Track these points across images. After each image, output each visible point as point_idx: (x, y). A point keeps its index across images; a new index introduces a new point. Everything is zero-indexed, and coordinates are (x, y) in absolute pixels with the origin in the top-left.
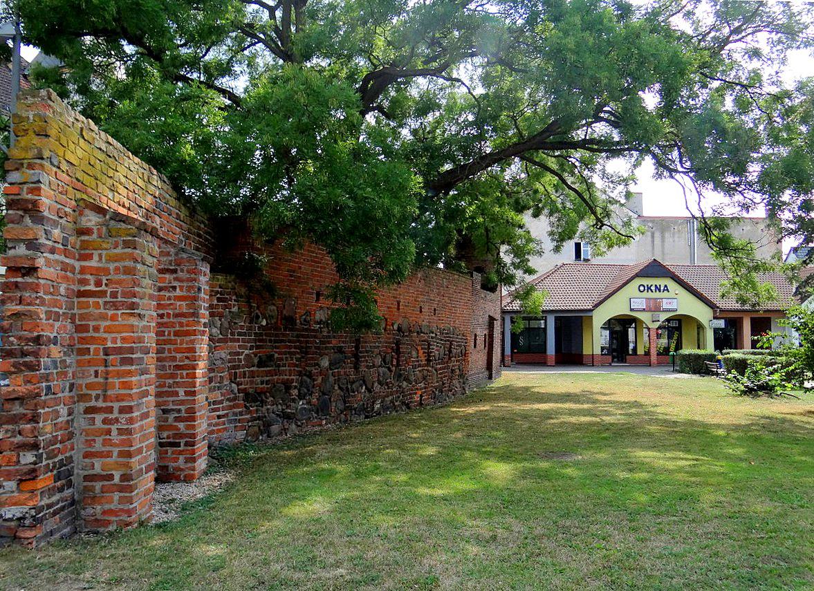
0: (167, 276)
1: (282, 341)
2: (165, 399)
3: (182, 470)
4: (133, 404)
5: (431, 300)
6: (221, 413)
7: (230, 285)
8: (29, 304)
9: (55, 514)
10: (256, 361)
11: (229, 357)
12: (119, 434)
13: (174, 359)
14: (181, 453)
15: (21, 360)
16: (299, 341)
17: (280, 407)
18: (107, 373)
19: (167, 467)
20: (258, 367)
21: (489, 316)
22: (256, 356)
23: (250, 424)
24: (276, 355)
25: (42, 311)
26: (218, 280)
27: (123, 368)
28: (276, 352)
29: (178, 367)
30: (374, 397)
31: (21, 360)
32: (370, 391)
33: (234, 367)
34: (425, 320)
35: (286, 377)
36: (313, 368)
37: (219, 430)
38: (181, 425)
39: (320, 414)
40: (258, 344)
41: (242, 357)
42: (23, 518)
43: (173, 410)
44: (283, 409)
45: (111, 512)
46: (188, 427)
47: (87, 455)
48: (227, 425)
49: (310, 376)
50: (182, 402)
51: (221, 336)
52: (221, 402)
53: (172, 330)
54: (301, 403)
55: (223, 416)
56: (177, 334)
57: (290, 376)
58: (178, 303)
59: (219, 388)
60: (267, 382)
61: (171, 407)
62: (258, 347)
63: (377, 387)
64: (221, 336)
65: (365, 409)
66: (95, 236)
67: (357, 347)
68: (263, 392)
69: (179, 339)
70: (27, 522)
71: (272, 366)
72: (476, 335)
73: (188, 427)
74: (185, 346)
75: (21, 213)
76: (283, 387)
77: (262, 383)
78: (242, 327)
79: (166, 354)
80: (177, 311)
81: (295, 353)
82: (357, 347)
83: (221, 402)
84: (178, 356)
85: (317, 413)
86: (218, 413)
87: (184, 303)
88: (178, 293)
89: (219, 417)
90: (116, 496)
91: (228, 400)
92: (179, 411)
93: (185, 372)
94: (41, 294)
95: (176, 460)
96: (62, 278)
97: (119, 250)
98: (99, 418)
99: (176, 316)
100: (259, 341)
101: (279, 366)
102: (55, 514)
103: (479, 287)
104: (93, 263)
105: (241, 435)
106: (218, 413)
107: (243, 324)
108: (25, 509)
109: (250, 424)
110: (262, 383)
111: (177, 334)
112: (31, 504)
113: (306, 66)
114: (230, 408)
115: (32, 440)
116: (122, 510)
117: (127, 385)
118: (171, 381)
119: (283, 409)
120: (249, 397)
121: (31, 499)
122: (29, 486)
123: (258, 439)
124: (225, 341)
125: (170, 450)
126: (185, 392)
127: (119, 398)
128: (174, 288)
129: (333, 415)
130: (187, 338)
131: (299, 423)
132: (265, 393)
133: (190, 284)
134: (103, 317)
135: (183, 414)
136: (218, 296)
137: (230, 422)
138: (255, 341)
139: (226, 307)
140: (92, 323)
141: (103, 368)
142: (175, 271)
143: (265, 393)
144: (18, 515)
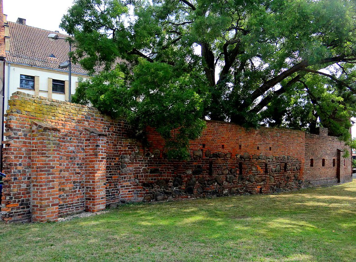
0: (88, 142)
1: (162, 163)
2: (87, 184)
3: (91, 208)
4: (42, 184)
5: (267, 143)
6: (130, 190)
7: (134, 142)
8: (9, 154)
9: (19, 215)
10: (149, 171)
11: (134, 169)
12: (40, 193)
13: (89, 170)
14: (91, 202)
15: (7, 170)
16: (173, 163)
17: (162, 189)
18: (37, 174)
19: (87, 207)
20: (150, 173)
21: (338, 149)
22: (149, 169)
23: (145, 195)
24: (160, 169)
25: (12, 157)
26: (128, 141)
27: (40, 173)
28: (160, 168)
29: (90, 173)
30: (223, 188)
31: (7, 170)
32: (220, 185)
33: (136, 173)
34: (262, 152)
35: (165, 178)
36: (182, 174)
37: (129, 197)
38: (91, 193)
39: (187, 193)
40: (149, 164)
41: (141, 170)
42: (6, 215)
43: (89, 187)
44: (164, 190)
45: (37, 217)
46: (93, 194)
47: (34, 199)
48: (133, 195)
49: (180, 177)
50: (91, 185)
51: (130, 162)
52: (130, 186)
53: (89, 160)
54: (175, 188)
55: (132, 191)
56: (90, 161)
57: (168, 177)
58: (90, 151)
59: (129, 181)
60: (155, 179)
61: (88, 186)
62: (149, 166)
63: (225, 183)
64: (130, 162)
65: (217, 193)
66: (35, 133)
67: (211, 166)
68: (152, 183)
69: (90, 163)
70: (7, 216)
71: (158, 173)
72: (324, 160)
73: (93, 194)
74: (92, 166)
75: (8, 128)
76: (165, 182)
77: (152, 179)
78: (141, 158)
79: (87, 169)
80: (90, 154)
81: (170, 168)
82: (211, 166)
83: (130, 186)
84: (90, 169)
85: (185, 192)
86: (129, 190)
87: (92, 151)
88: (90, 147)
89: (129, 191)
90: (39, 212)
91: (133, 185)
92: (90, 188)
93: (92, 175)
94: (12, 151)
95: (90, 204)
96: (23, 146)
97: (40, 137)
98: (36, 188)
99: (90, 155)
100: (150, 163)
101: (161, 173)
102: (19, 215)
103: (326, 135)
104: (35, 141)
105: (141, 199)
106: (129, 190)
107: (141, 157)
108: (6, 212)
109: (145, 195)
110: (152, 179)
111: (90, 161)
112: (8, 211)
113: (172, 49)
114: (135, 188)
115: (8, 193)
116: (40, 217)
117: (41, 178)
118: (88, 177)
119: (164, 190)
120: (144, 185)
121: (8, 209)
122: (8, 206)
123: (150, 201)
124: (133, 163)
125: (88, 201)
126: (92, 181)
127: (40, 182)
128: (89, 146)
129: (195, 194)
130: (92, 163)
131: (174, 196)
132: (154, 183)
133: (93, 144)
134: (36, 157)
135: (92, 189)
136: (129, 147)
137: (135, 193)
138: (148, 163)
139: (132, 151)
140: (34, 159)
141: (36, 173)
142: (89, 140)
143: (154, 183)
144: (5, 214)
